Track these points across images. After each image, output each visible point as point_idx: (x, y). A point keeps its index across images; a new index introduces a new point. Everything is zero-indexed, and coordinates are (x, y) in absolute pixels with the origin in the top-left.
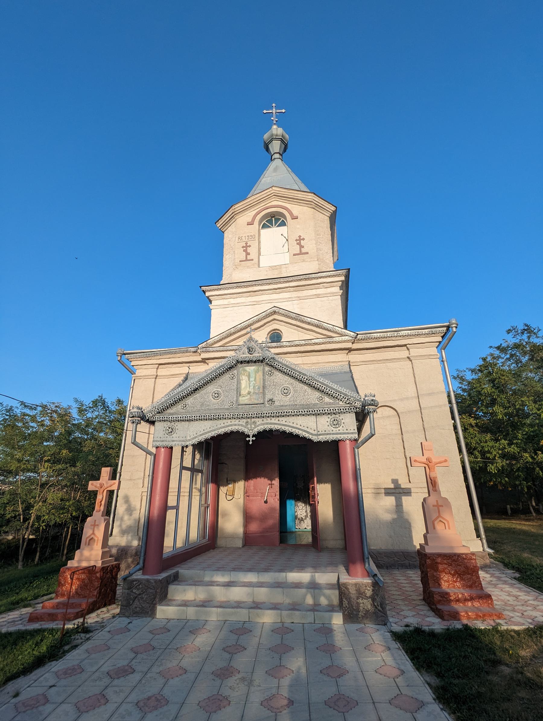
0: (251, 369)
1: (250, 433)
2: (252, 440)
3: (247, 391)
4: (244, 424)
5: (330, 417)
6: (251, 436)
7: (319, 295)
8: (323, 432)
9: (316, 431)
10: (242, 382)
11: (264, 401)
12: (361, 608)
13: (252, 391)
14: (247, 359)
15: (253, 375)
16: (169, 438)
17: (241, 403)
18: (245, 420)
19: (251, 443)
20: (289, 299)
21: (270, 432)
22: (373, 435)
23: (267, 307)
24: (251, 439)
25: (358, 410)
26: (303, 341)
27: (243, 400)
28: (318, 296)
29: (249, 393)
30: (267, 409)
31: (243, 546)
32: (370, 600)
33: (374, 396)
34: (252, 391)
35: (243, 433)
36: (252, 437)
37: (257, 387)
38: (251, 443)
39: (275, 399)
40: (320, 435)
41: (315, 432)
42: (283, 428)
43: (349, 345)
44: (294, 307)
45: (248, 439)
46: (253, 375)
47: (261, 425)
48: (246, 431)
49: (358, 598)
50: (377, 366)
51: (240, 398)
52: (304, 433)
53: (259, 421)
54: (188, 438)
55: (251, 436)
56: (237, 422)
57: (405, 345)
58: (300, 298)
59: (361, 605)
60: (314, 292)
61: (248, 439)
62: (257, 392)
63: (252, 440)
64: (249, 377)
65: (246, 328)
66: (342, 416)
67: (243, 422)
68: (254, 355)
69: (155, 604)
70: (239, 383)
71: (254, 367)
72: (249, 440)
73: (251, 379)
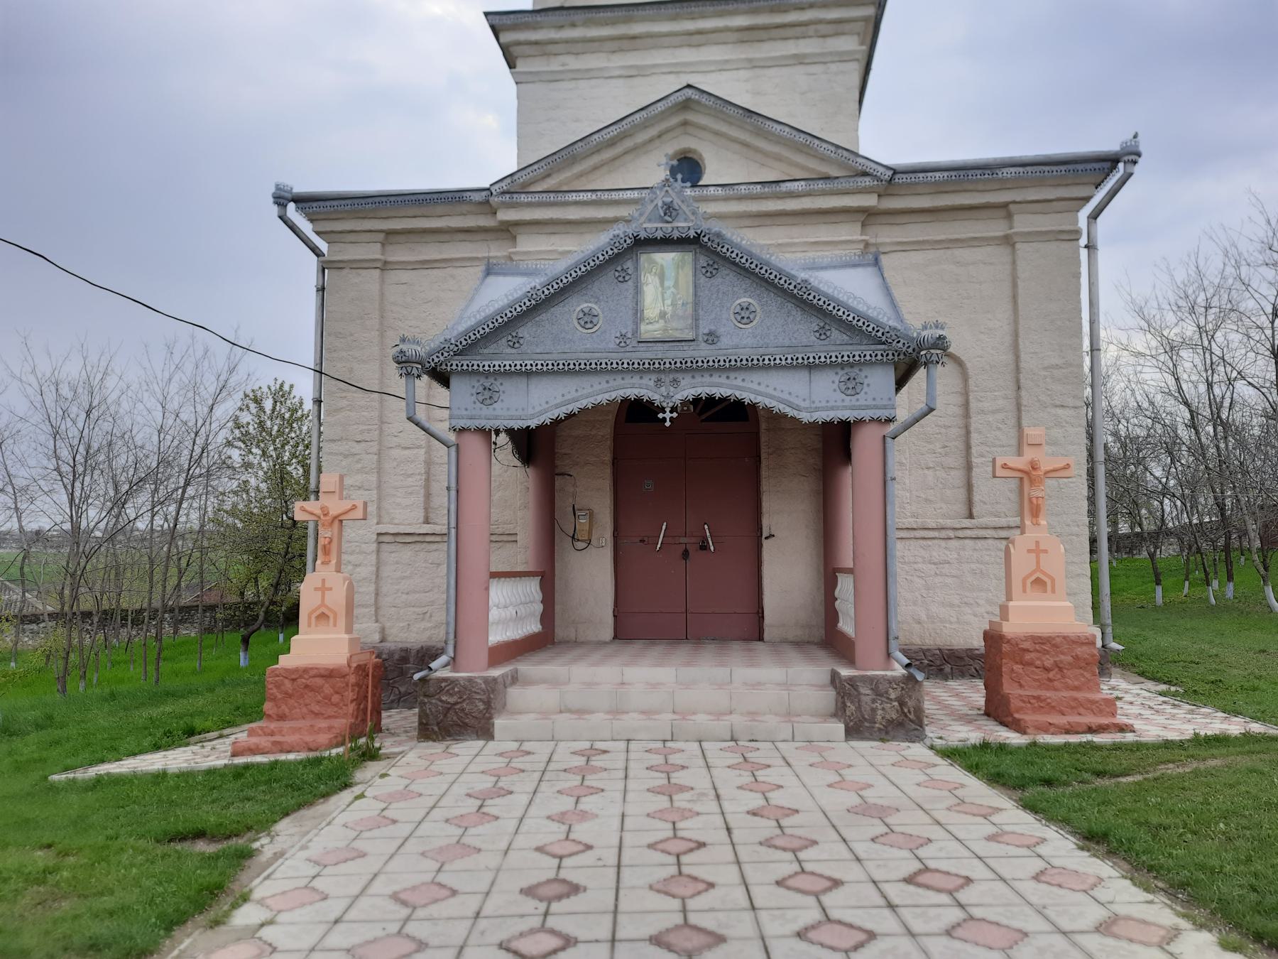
0: (666, 259)
1: (664, 405)
2: (671, 418)
3: (657, 312)
4: (652, 383)
5: (841, 372)
6: (668, 410)
7: (805, 56)
8: (824, 404)
9: (807, 402)
10: (645, 288)
11: (697, 335)
12: (879, 718)
13: (669, 310)
14: (659, 235)
15: (670, 273)
16: (486, 411)
17: (645, 337)
18: (654, 377)
19: (668, 424)
20: (723, 66)
21: (711, 400)
22: (932, 410)
23: (667, 85)
24: (668, 415)
25: (902, 357)
26: (759, 187)
27: (650, 330)
28: (800, 60)
29: (663, 315)
30: (703, 352)
31: (615, 637)
32: (896, 704)
33: (942, 328)
34: (669, 310)
35: (650, 403)
36: (671, 412)
37: (680, 302)
38: (668, 424)
39: (721, 330)
40: (817, 409)
41: (806, 404)
42: (739, 395)
43: (870, 201)
44: (732, 87)
45: (661, 416)
46: (670, 273)
47: (689, 388)
48: (656, 397)
49: (874, 701)
50: (931, 255)
51: (643, 327)
52: (781, 407)
53: (685, 380)
54: (531, 411)
55: (668, 410)
56: (636, 380)
57: (1005, 206)
58: (753, 64)
59: (880, 712)
60: (791, 48)
61: (661, 416)
62: (680, 312)
63: (671, 418)
64: (662, 278)
65: (612, 143)
66: (867, 371)
67: (649, 380)
68: (676, 224)
69: (491, 718)
70: (638, 290)
71: (672, 255)
72: (664, 419)
73: (667, 284)
